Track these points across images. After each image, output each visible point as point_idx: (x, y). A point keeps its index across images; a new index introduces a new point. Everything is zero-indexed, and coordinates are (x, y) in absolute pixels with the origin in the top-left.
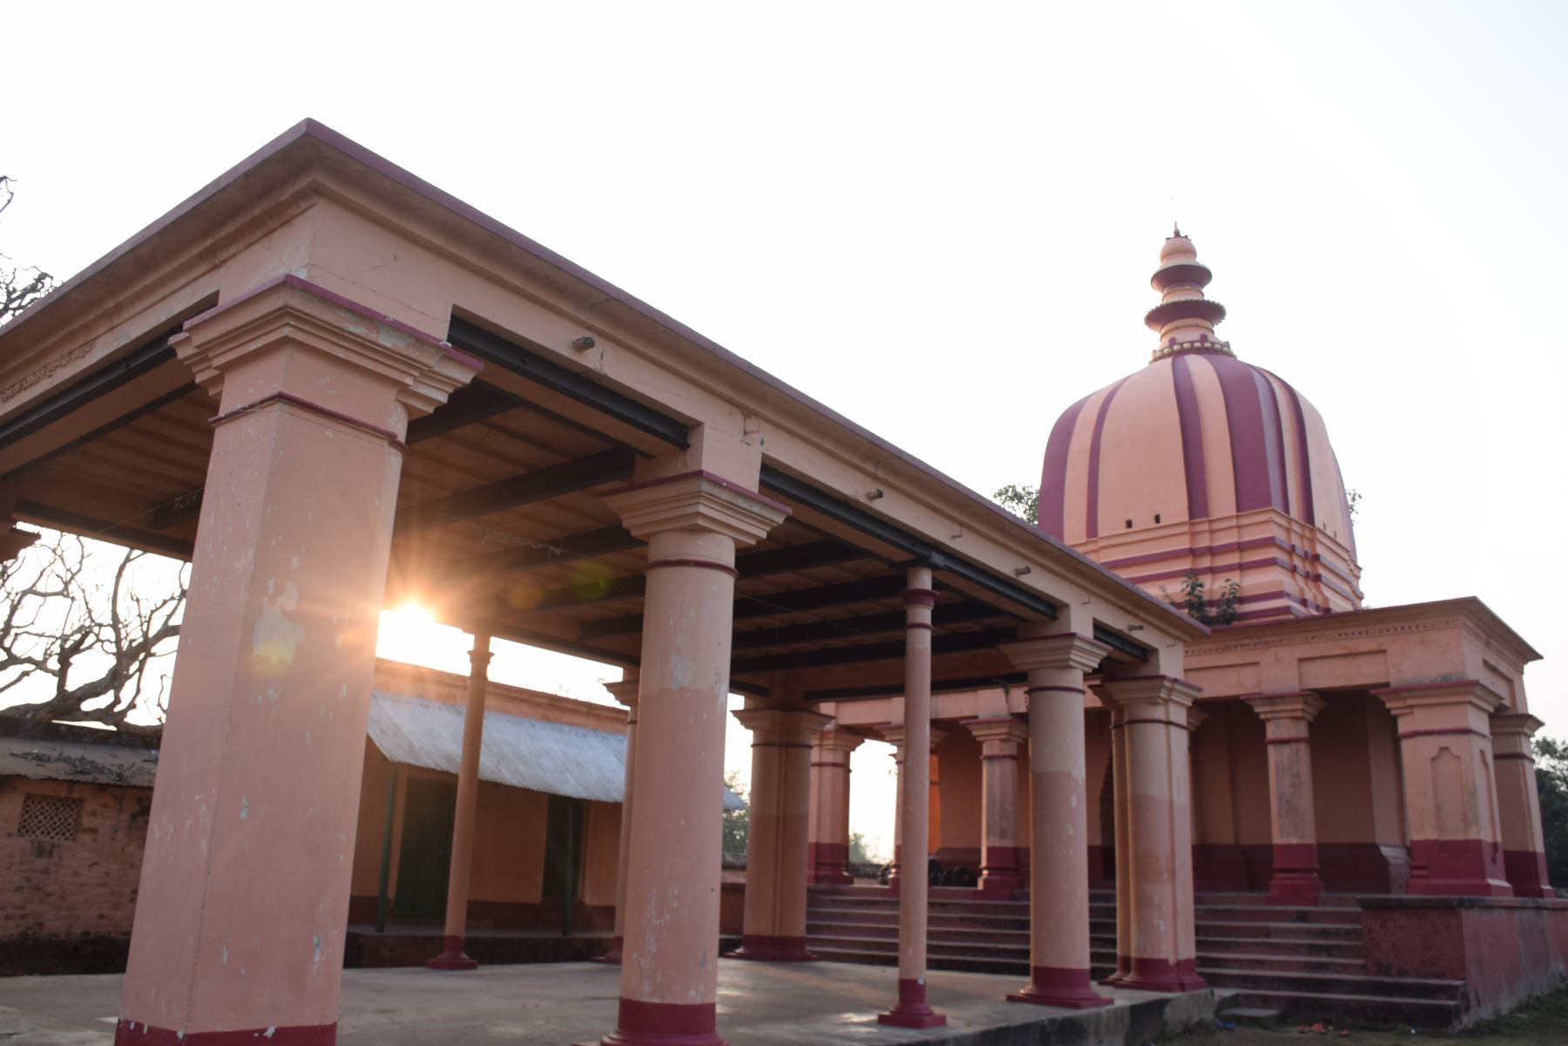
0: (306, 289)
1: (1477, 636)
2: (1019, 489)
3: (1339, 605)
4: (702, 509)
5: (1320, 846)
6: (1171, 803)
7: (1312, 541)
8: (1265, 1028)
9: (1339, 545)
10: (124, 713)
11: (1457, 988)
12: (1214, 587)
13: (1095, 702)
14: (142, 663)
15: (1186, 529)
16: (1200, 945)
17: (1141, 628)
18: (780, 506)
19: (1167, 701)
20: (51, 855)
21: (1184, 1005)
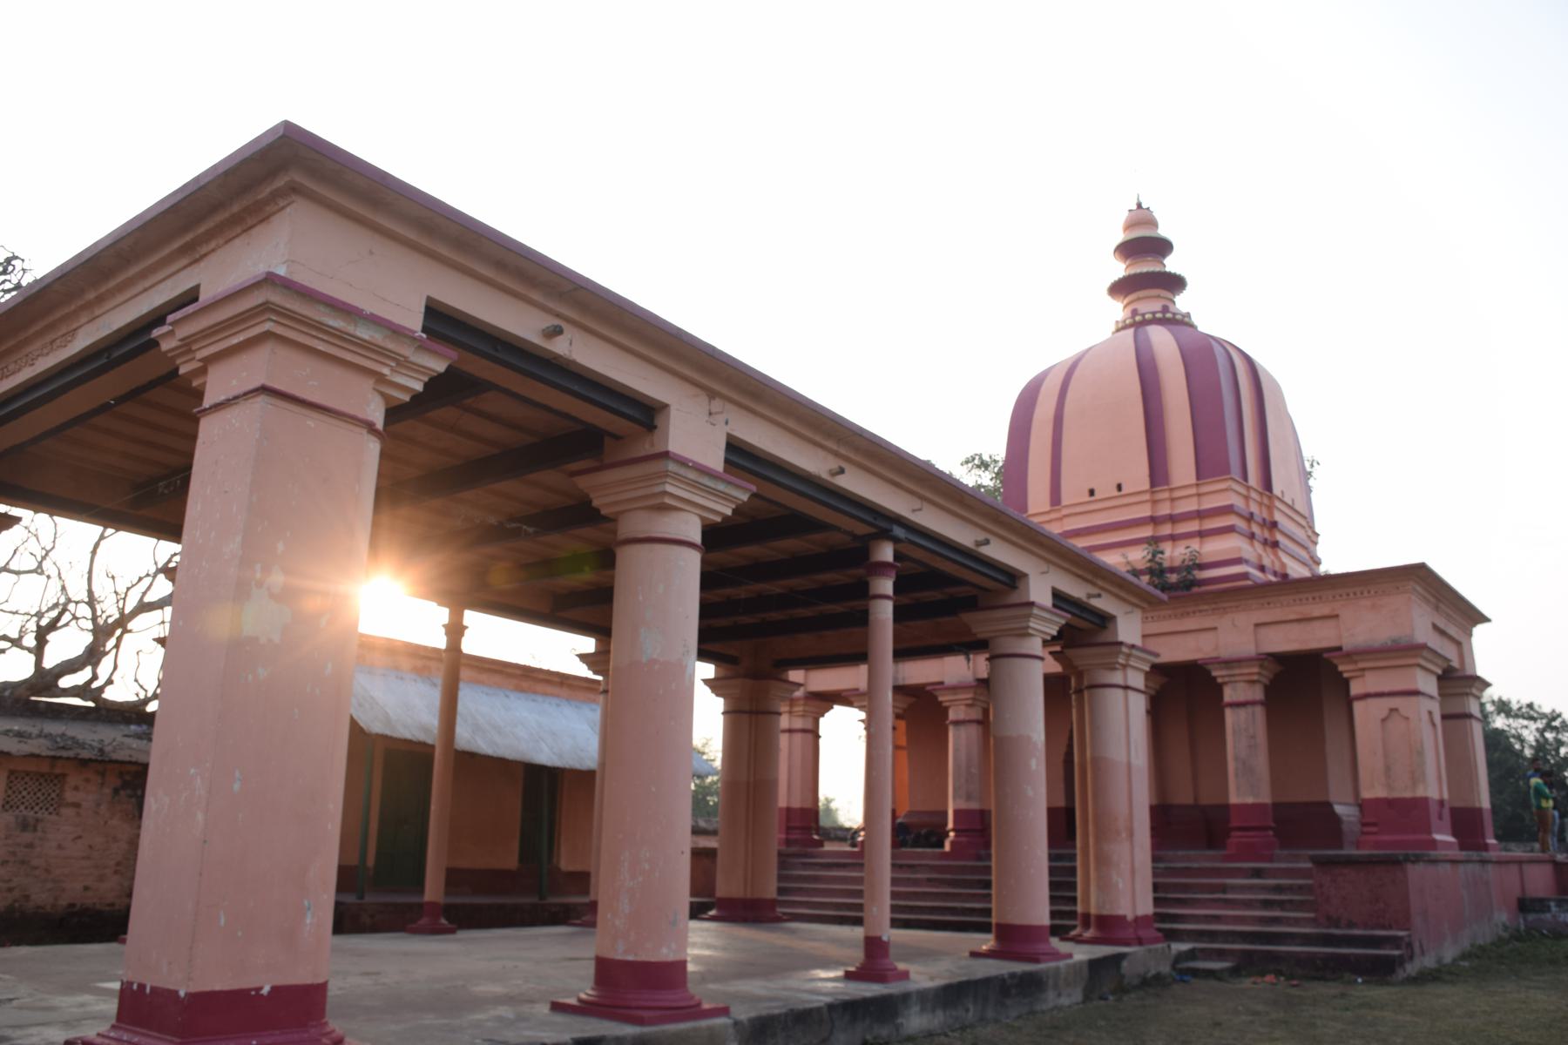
0: (286, 285)
1: (1427, 601)
2: (986, 458)
3: (1297, 571)
4: (669, 488)
5: (1275, 805)
6: (1129, 765)
7: (1270, 508)
8: (1220, 979)
9: (1297, 512)
10: (101, 689)
11: (1401, 938)
12: (1174, 554)
13: (1055, 667)
14: (119, 639)
15: (1147, 497)
16: (1157, 902)
17: (1099, 596)
18: (744, 484)
19: (1125, 667)
20: (35, 830)
21: (1140, 958)
